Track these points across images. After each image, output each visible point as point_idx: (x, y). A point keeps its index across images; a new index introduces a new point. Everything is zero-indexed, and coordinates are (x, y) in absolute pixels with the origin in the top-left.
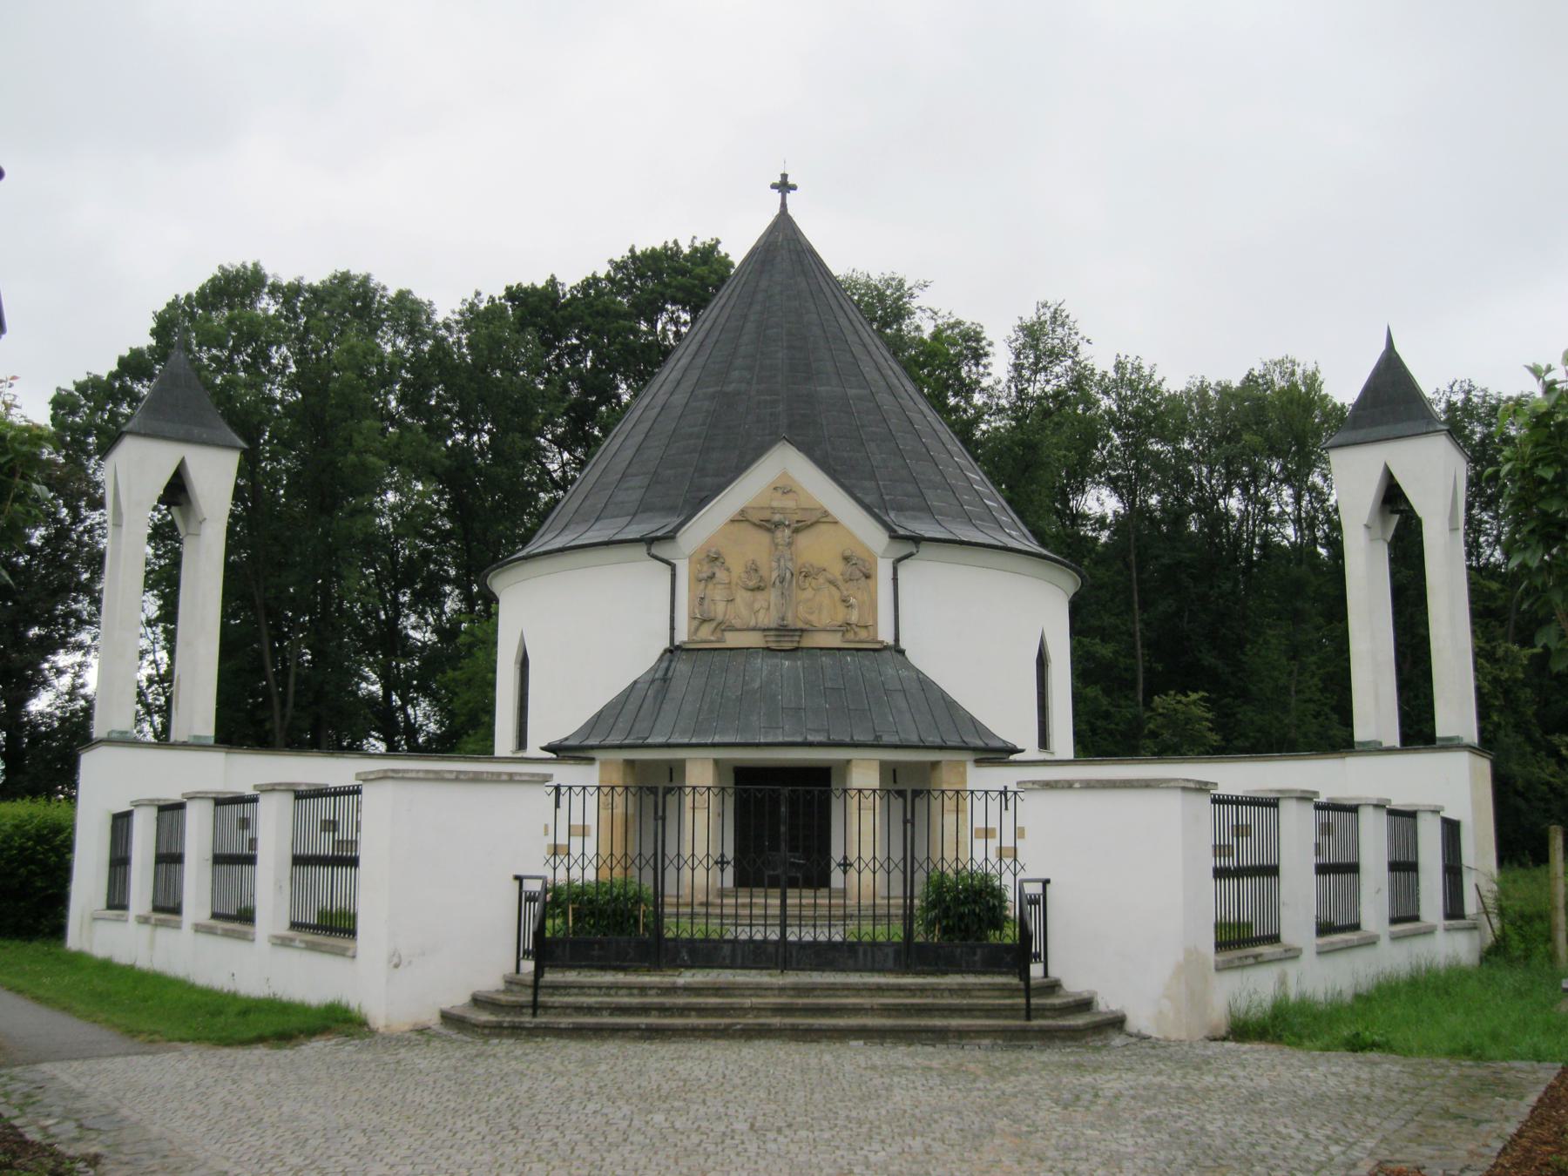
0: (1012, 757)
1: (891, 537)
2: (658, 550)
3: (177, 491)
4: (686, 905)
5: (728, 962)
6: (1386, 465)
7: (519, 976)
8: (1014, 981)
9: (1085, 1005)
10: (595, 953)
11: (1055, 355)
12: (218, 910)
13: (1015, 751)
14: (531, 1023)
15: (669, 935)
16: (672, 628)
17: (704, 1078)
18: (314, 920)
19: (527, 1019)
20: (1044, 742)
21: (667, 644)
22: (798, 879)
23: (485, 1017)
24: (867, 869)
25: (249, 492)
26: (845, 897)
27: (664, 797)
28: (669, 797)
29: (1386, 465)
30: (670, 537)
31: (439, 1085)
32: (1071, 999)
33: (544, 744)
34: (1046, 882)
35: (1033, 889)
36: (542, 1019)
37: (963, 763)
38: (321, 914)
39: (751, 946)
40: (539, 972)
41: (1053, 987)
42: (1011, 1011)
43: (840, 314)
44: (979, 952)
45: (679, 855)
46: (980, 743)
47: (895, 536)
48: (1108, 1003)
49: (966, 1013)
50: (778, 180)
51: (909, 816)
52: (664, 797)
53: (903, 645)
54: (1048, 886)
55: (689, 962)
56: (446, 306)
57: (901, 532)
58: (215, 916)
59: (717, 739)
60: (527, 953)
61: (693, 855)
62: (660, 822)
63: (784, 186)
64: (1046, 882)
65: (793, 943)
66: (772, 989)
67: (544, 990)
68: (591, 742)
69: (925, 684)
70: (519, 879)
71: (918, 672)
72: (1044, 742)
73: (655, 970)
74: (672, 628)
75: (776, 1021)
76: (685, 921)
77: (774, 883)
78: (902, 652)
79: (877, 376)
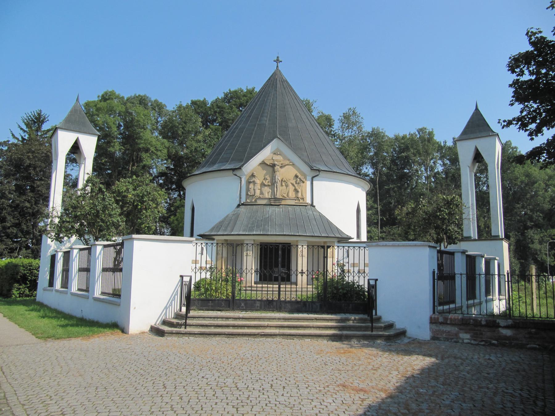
0: (350, 240)
1: (311, 169)
2: (236, 172)
3: (76, 148)
4: (249, 287)
5: (259, 308)
6: (476, 147)
7: (181, 313)
8: (366, 316)
9: (390, 326)
10: (210, 304)
11: (354, 124)
12: (80, 288)
13: (351, 238)
14: (184, 331)
15: (237, 298)
16: (240, 198)
17: (250, 358)
18: (111, 292)
19: (182, 330)
20: (358, 236)
21: (238, 203)
22: (287, 278)
23: (166, 328)
24: (310, 275)
25: (101, 151)
26: (296, 285)
27: (236, 247)
28: (238, 247)
29: (476, 147)
30: (240, 168)
31: (86, 403)
32: (387, 324)
33: (198, 234)
34: (376, 280)
35: (372, 283)
36: (189, 329)
37: (334, 242)
38: (114, 290)
39: (268, 302)
40: (188, 310)
41: (379, 319)
42: (366, 329)
43: (295, 101)
44: (351, 305)
45: (241, 268)
46: (340, 236)
47: (312, 169)
48: (399, 326)
49: (348, 329)
50: (276, 59)
51: (326, 256)
52: (236, 247)
53: (314, 204)
54: (377, 282)
55: (244, 308)
56: (171, 106)
57: (315, 168)
58: (79, 290)
59: (254, 233)
60: (184, 305)
61: (246, 268)
62: (234, 257)
63: (278, 61)
64: (376, 280)
65: (283, 301)
66: (275, 319)
67: (167, 334)
68: (213, 233)
69: (322, 217)
70: (182, 277)
71: (319, 213)
72: (358, 236)
73: (232, 311)
74: (240, 198)
75: (277, 331)
76: (243, 292)
77: (276, 279)
78: (314, 206)
79: (307, 120)
